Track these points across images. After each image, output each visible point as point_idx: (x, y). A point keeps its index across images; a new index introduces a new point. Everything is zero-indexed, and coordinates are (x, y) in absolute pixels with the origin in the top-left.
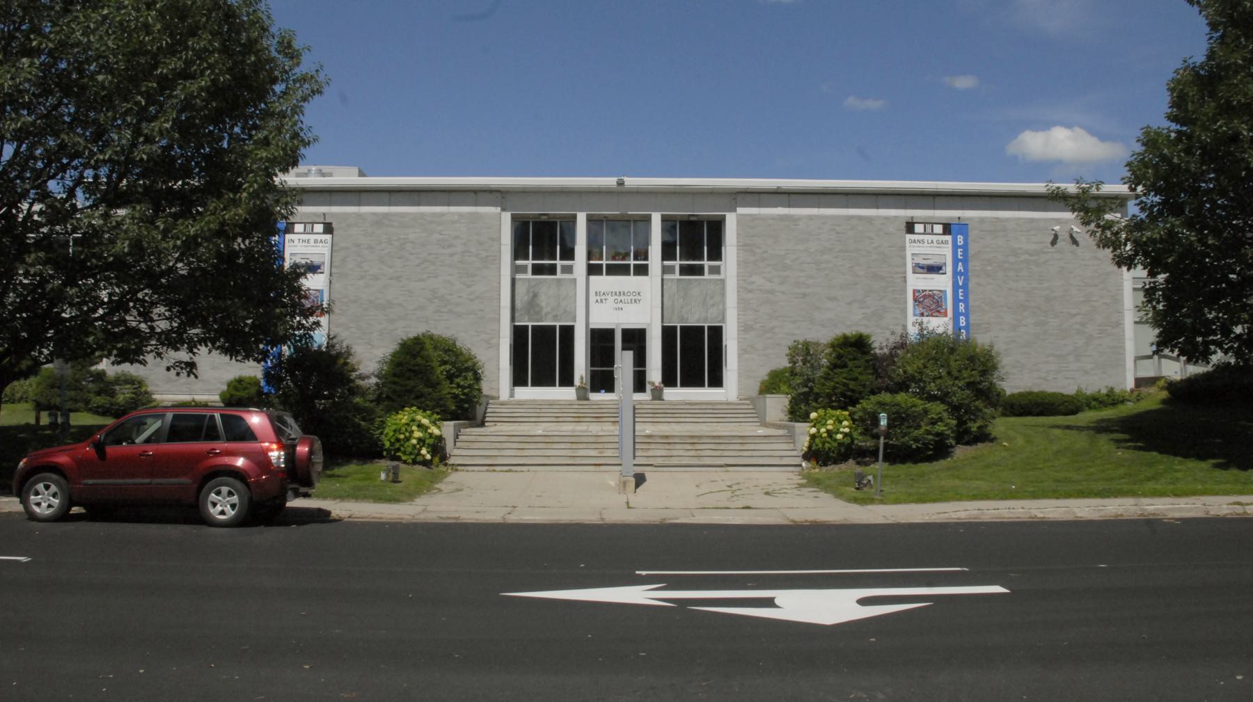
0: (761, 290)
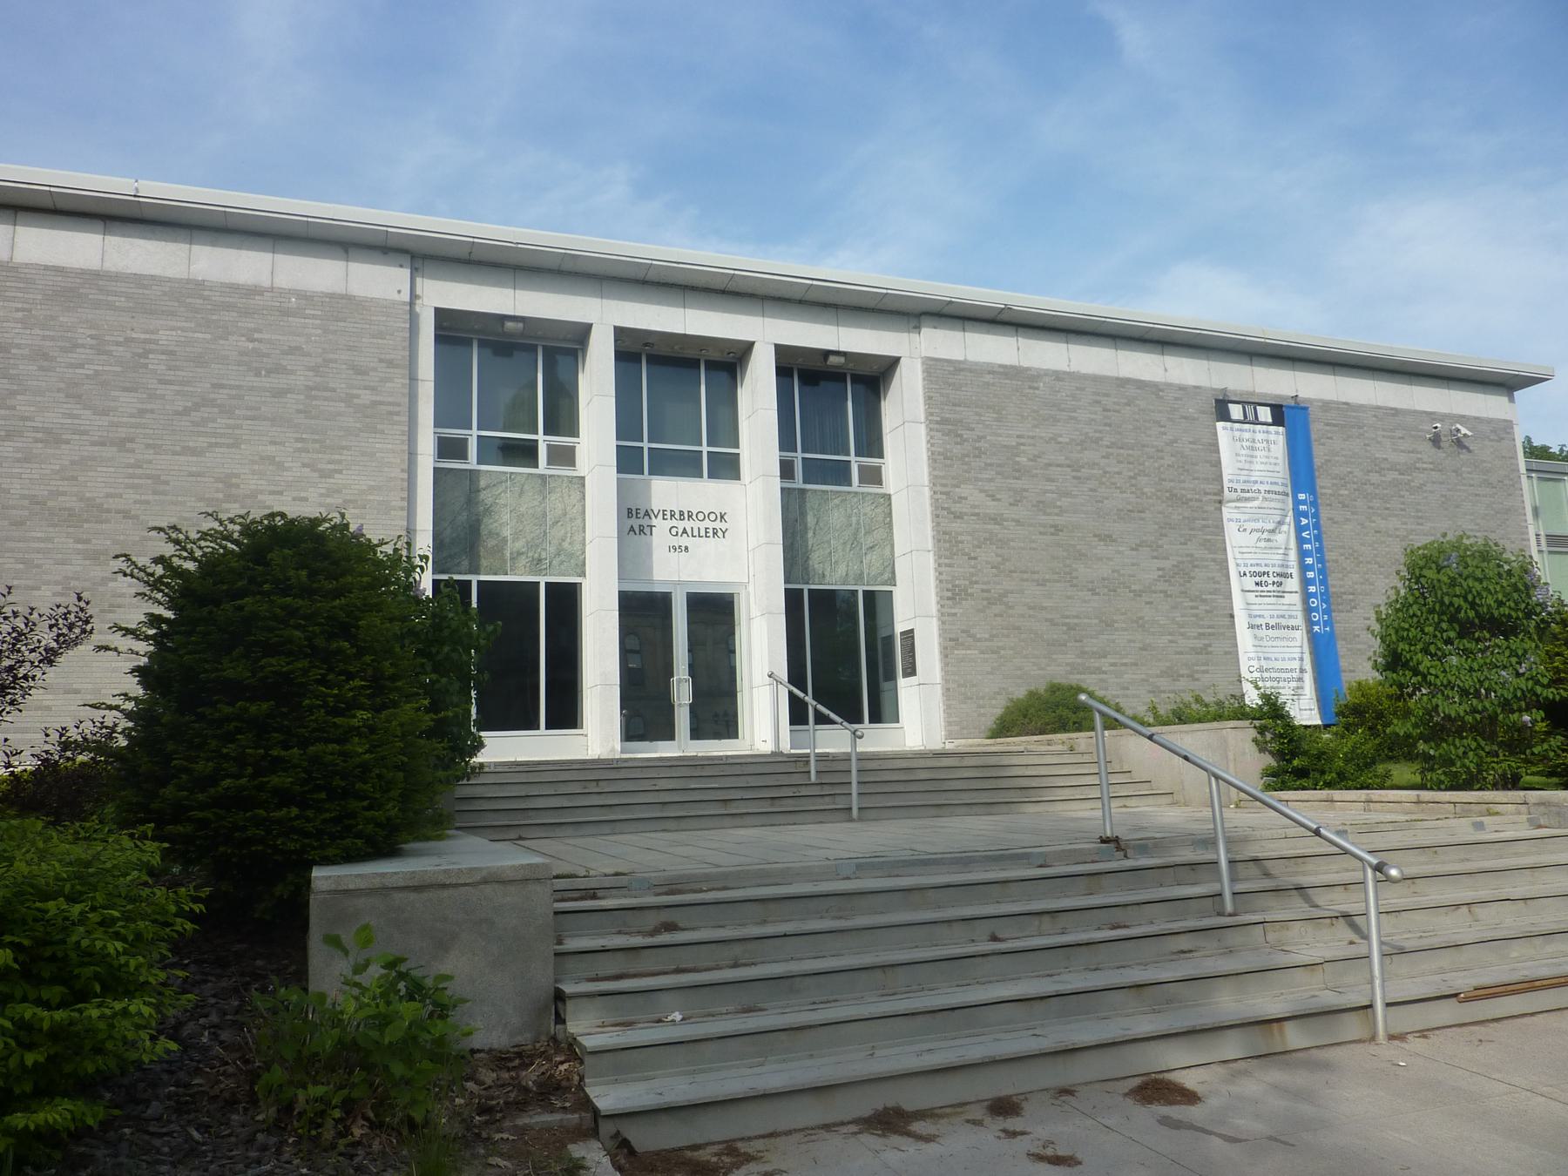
0: (977, 515)
